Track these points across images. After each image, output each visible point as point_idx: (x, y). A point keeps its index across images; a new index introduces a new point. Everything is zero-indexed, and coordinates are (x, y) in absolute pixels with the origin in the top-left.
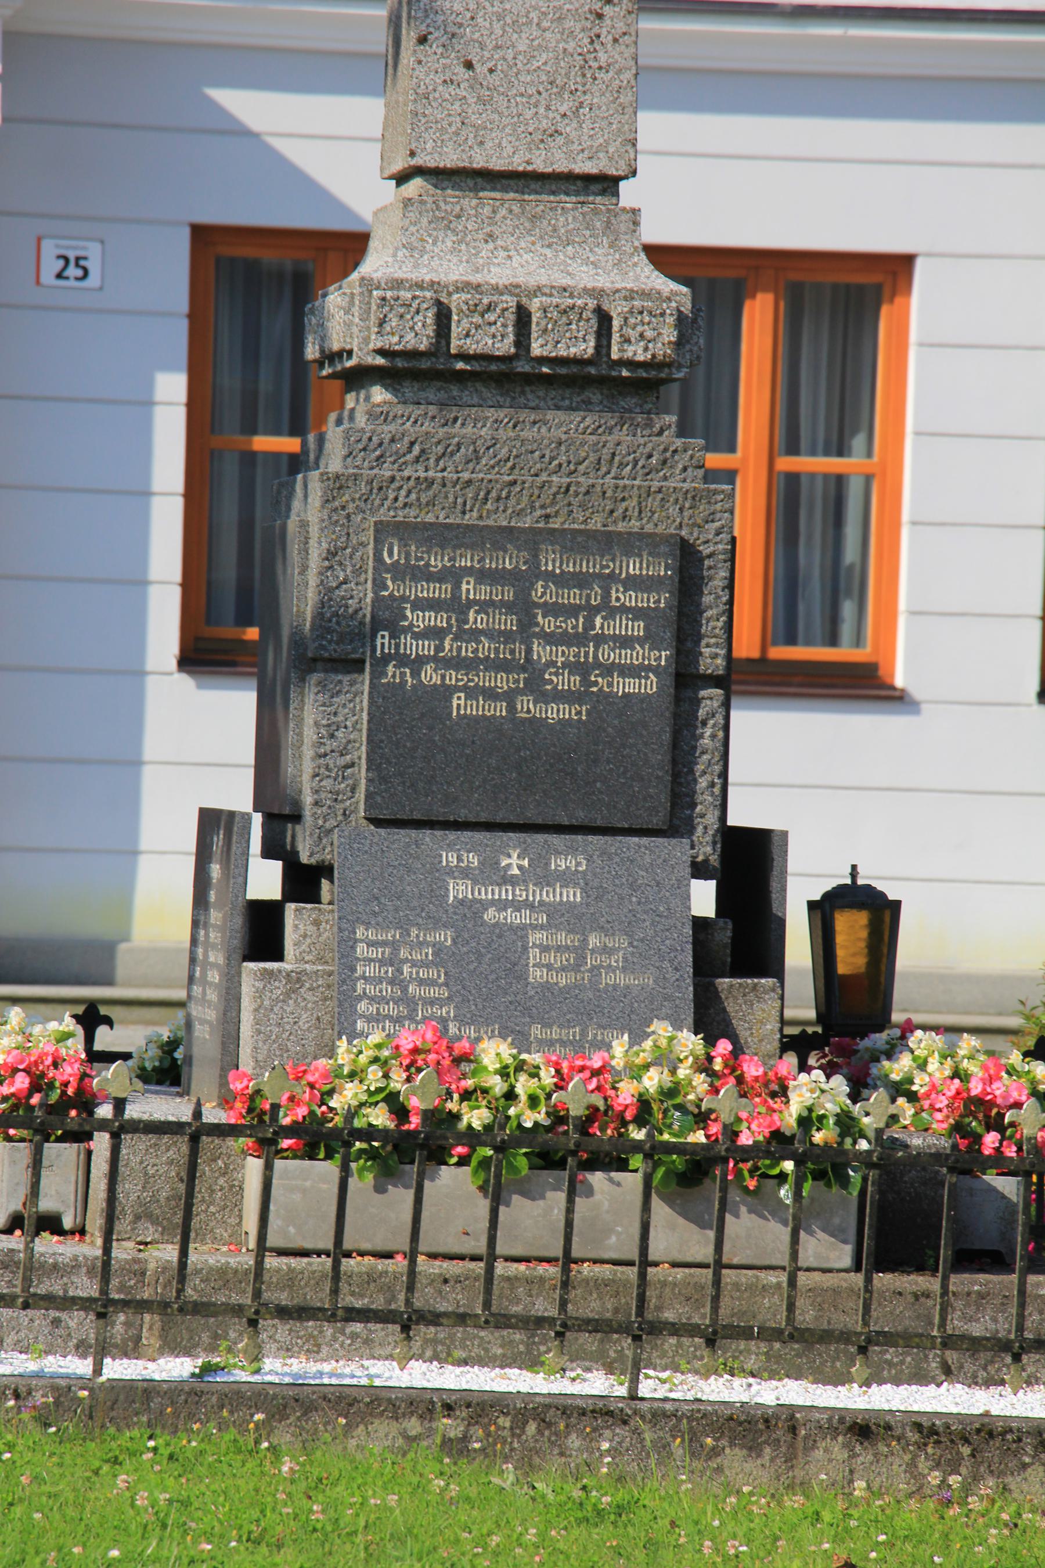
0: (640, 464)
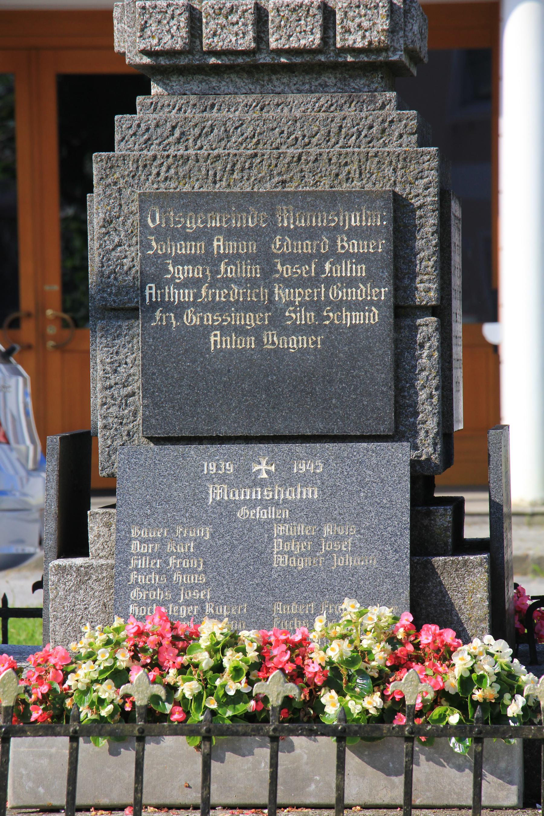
0: (363, 134)
